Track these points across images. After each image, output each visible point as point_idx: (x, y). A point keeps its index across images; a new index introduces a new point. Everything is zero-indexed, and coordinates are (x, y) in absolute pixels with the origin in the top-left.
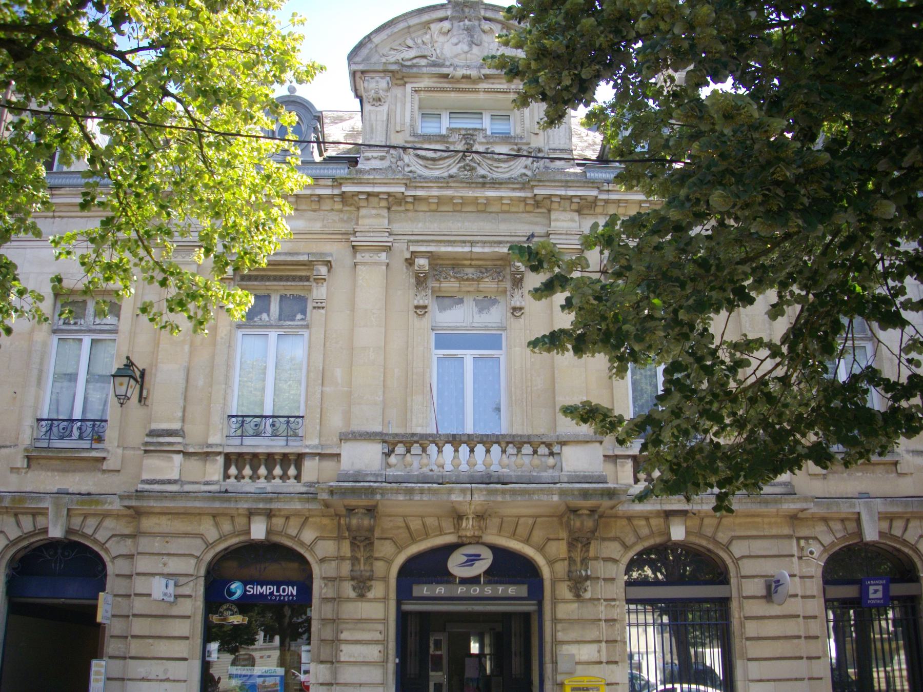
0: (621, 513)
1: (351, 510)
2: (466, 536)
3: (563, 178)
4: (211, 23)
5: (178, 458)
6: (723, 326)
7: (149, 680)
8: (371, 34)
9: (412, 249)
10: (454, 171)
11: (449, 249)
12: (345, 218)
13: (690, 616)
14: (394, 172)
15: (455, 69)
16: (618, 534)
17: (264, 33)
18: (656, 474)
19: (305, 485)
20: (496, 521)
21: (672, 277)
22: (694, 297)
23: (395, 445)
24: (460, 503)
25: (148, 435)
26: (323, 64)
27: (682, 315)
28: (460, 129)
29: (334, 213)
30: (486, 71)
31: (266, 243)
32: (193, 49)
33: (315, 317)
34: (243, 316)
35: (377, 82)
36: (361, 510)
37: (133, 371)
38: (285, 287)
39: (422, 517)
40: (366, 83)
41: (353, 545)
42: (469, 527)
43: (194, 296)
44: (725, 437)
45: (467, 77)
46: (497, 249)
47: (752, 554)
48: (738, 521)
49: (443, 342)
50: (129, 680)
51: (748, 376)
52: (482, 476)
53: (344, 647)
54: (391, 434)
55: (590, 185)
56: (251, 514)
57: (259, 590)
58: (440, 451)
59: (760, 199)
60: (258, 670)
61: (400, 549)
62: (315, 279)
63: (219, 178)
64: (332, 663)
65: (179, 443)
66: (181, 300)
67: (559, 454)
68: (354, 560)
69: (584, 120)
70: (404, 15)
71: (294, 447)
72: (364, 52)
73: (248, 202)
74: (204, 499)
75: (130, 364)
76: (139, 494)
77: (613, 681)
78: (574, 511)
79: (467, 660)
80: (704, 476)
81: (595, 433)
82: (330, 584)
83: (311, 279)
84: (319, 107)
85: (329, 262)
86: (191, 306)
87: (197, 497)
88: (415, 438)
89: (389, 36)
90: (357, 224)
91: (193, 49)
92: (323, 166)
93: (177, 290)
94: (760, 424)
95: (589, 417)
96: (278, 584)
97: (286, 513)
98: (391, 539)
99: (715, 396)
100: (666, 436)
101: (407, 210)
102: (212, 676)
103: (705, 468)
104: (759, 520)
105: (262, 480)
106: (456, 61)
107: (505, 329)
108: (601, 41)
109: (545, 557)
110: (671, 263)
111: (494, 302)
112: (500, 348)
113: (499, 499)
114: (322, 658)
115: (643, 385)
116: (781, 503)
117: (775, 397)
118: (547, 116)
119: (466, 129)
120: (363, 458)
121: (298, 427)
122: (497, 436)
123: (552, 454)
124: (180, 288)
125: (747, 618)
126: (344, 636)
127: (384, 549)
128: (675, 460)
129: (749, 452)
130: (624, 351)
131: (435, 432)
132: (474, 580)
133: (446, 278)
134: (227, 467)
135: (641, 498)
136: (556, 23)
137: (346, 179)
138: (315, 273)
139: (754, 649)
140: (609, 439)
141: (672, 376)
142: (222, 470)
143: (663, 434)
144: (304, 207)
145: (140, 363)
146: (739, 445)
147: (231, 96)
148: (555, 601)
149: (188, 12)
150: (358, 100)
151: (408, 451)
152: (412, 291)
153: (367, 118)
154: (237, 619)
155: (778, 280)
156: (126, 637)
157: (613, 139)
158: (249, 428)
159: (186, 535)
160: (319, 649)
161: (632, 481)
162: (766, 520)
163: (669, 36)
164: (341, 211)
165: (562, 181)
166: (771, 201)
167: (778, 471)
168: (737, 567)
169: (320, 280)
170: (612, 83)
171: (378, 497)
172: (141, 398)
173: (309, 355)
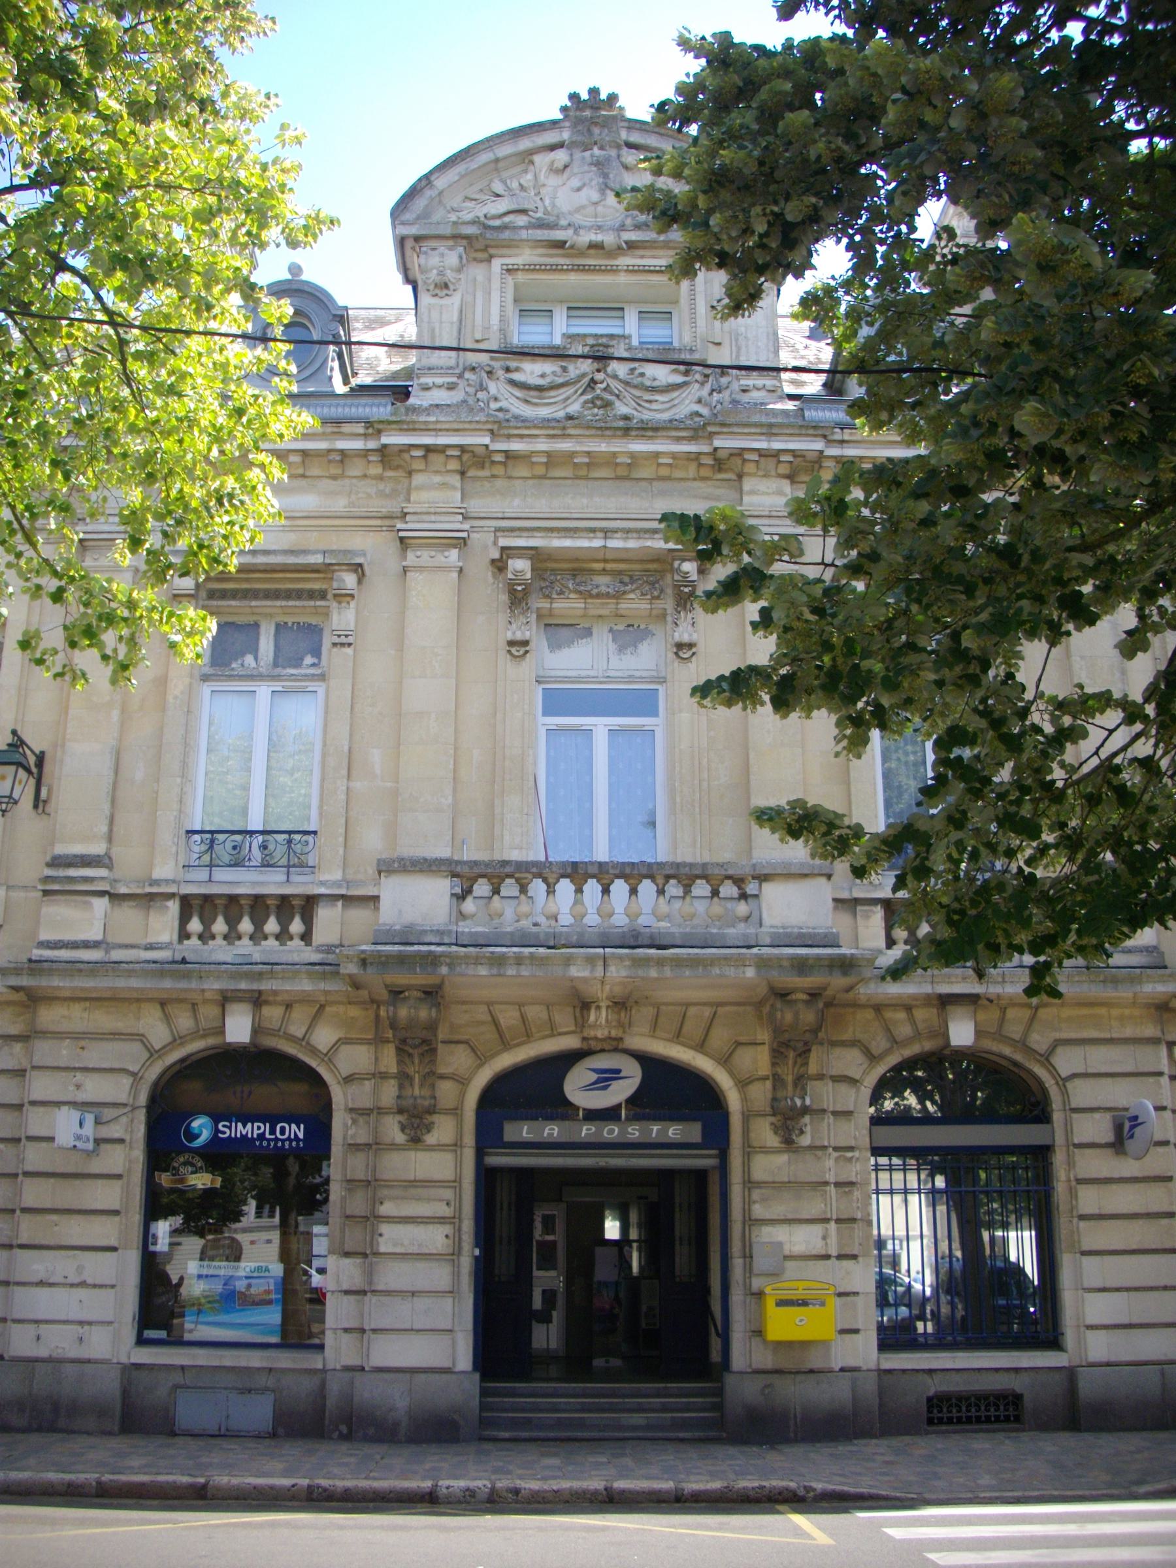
0: (863, 999)
1: (396, 994)
2: (596, 1038)
3: (764, 419)
4: (138, 141)
5: (101, 905)
6: (1044, 669)
7: (51, 1285)
8: (431, 172)
9: (503, 542)
10: (575, 408)
11: (567, 543)
12: (387, 491)
13: (983, 1175)
14: (471, 410)
15: (576, 232)
16: (859, 1036)
17: (229, 158)
18: (924, 929)
19: (318, 950)
20: (648, 1012)
21: (950, 574)
22: (990, 609)
23: (474, 880)
24: (585, 980)
25: (48, 865)
26: (334, 214)
27: (968, 640)
28: (585, 336)
29: (368, 481)
30: (633, 236)
31: (237, 528)
32: (107, 187)
33: (335, 659)
34: (198, 656)
35: (442, 255)
36: (416, 994)
37: (24, 755)
38: (275, 610)
39: (520, 1005)
40: (422, 257)
41: (400, 1051)
42: (600, 1021)
43: (110, 619)
44: (1046, 867)
45: (595, 246)
46: (649, 543)
47: (1090, 1071)
48: (1066, 1012)
49: (556, 703)
50: (18, 1284)
51: (1084, 753)
52: (623, 935)
53: (385, 1228)
54: (465, 863)
55: (811, 432)
56: (226, 999)
57: (241, 1130)
58: (551, 891)
59: (1105, 419)
60: (246, 1266)
61: (482, 1059)
62: (335, 596)
63: (155, 413)
64: (365, 1255)
65: (102, 878)
66: (89, 626)
67: (756, 896)
68: (404, 1078)
69: (797, 308)
70: (488, 140)
71: (300, 885)
72: (420, 204)
73: (206, 458)
74: (146, 974)
75: (18, 743)
76: (35, 966)
77: (848, 1289)
78: (782, 995)
79: (599, 1251)
80: (1005, 930)
81: (813, 856)
82: (361, 1120)
83: (330, 596)
84: (341, 299)
85: (360, 565)
86: (109, 638)
87: (133, 971)
88: (508, 870)
89: (462, 177)
90: (408, 501)
91: (107, 187)
92: (349, 401)
93: (82, 609)
94: (1106, 840)
95: (802, 828)
96: (272, 1119)
97: (286, 997)
98: (466, 1042)
99: (1024, 790)
100: (938, 862)
101: (493, 476)
102: (165, 1278)
103: (1007, 917)
104: (1103, 1011)
105: (246, 941)
106: (578, 219)
107: (663, 681)
108: (819, 148)
109: (731, 1073)
110: (950, 550)
111: (646, 634)
112: (656, 715)
113: (653, 973)
114: (347, 1248)
115: (903, 780)
116: (1140, 983)
117: (1133, 794)
118: (729, 296)
119: (596, 336)
120: (419, 903)
121: (306, 849)
122: (650, 865)
123: (744, 896)
124: (87, 605)
125: (1080, 1181)
126: (386, 1209)
127: (455, 1060)
128: (956, 905)
129: (1087, 890)
130: (863, 709)
131: (543, 859)
132: (609, 1114)
133: (561, 593)
134: (184, 919)
135: (897, 972)
136: (742, 126)
137: (390, 423)
138: (335, 585)
139: (1094, 1236)
140: (841, 867)
141: (950, 752)
142: (176, 924)
143: (932, 857)
144: (315, 471)
145: (36, 742)
146: (1068, 878)
147: (173, 269)
148: (749, 1151)
149: (97, 122)
150: (409, 288)
151: (496, 891)
152: (503, 617)
153: (426, 319)
154: (201, 1181)
155: (1140, 585)
156: (13, 1211)
157: (849, 342)
158: (224, 849)
159: (116, 1036)
160: (343, 1231)
161: (882, 943)
162: (1115, 1012)
163: (942, 135)
164: (380, 478)
165: (761, 425)
166: (1126, 424)
167: (1137, 923)
168: (1064, 1092)
169: (344, 597)
170: (845, 241)
171: (444, 970)
172: (37, 802)
173: (325, 725)
